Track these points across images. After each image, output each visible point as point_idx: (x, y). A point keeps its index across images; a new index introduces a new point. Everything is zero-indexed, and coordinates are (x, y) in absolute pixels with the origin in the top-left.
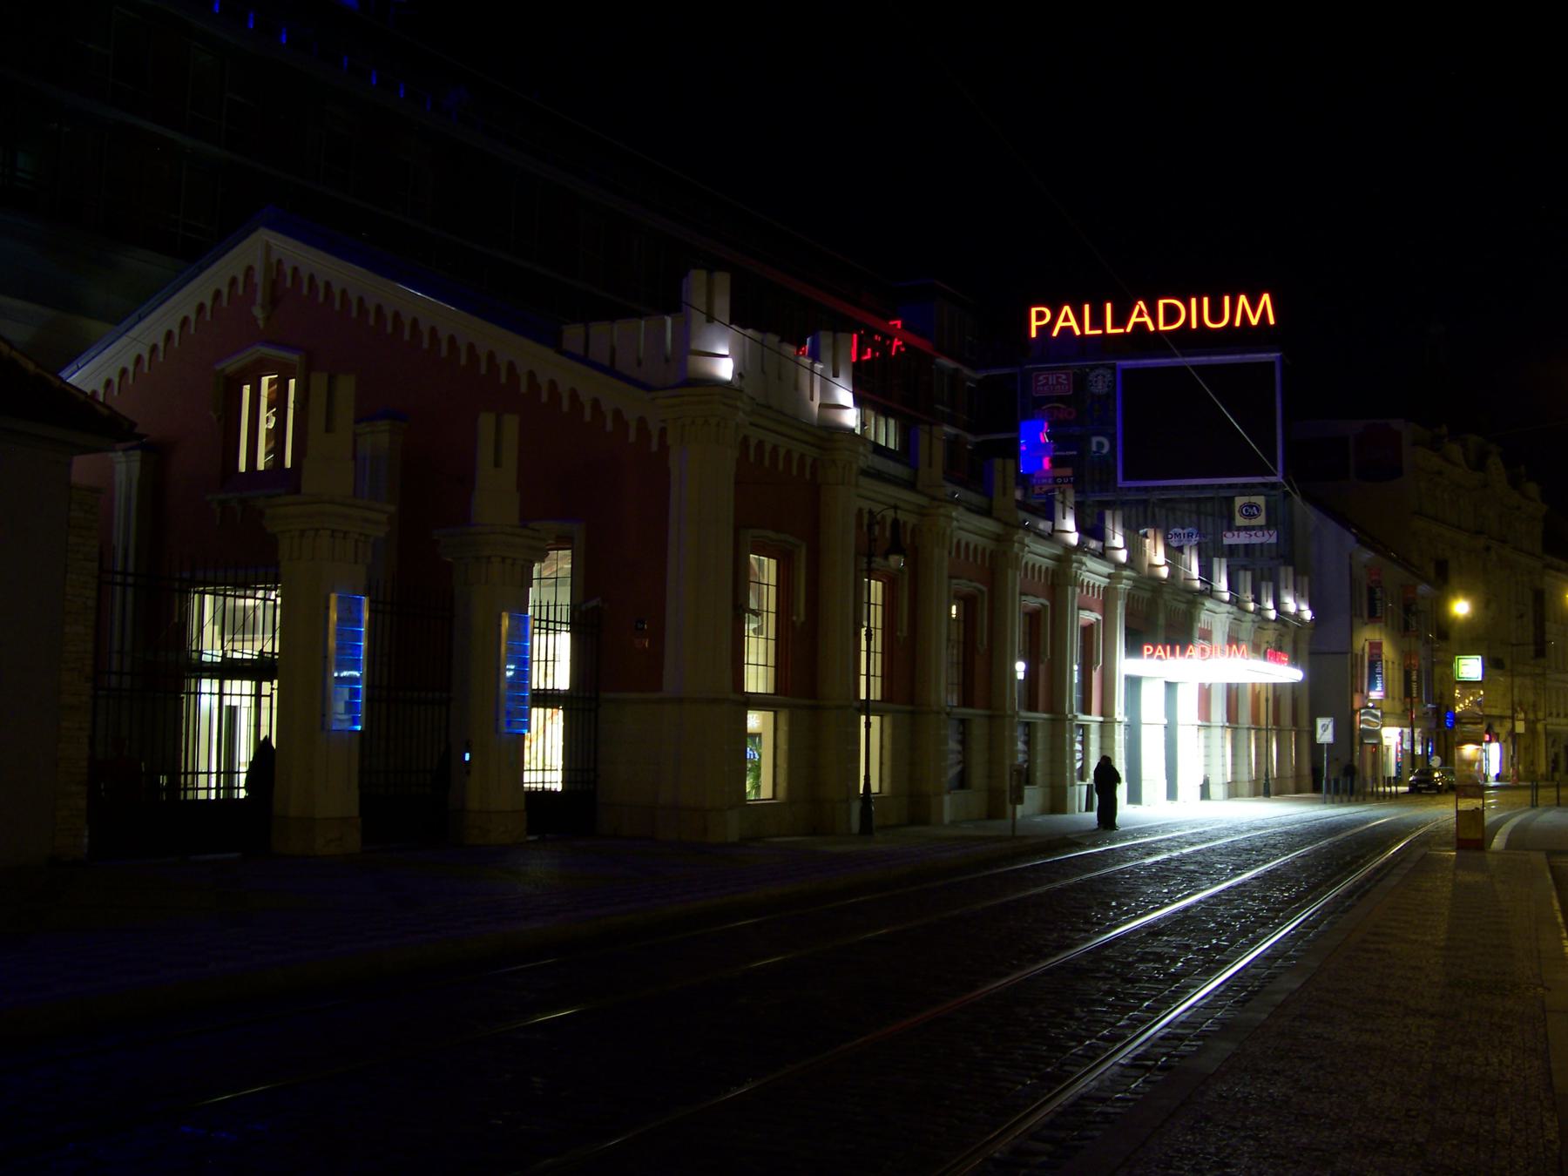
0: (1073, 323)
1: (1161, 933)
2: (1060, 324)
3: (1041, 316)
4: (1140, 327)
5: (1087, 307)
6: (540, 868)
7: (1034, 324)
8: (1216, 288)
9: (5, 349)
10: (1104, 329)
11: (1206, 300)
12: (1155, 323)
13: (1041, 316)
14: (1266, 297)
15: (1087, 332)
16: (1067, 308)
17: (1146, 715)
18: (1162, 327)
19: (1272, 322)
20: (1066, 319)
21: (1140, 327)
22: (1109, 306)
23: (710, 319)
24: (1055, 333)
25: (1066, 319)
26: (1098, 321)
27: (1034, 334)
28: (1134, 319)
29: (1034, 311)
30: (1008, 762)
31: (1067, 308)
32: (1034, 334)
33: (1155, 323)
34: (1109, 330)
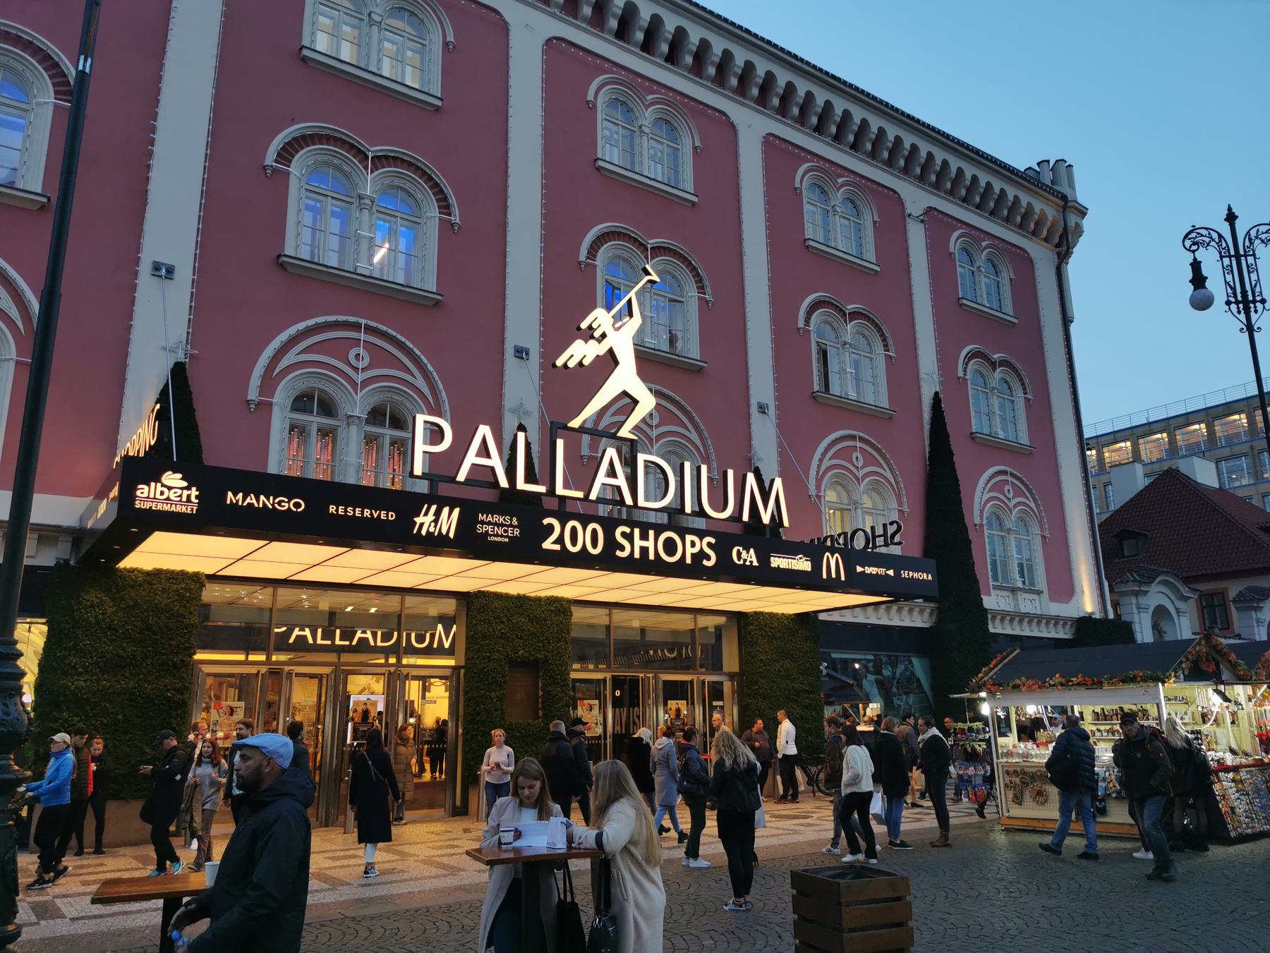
2: (471, 458)
10: (333, 641)
13: (435, 434)
16: (484, 431)
22: (392, 516)
24: (291, 641)
28: (601, 478)
31: (484, 431)
34: (560, 490)
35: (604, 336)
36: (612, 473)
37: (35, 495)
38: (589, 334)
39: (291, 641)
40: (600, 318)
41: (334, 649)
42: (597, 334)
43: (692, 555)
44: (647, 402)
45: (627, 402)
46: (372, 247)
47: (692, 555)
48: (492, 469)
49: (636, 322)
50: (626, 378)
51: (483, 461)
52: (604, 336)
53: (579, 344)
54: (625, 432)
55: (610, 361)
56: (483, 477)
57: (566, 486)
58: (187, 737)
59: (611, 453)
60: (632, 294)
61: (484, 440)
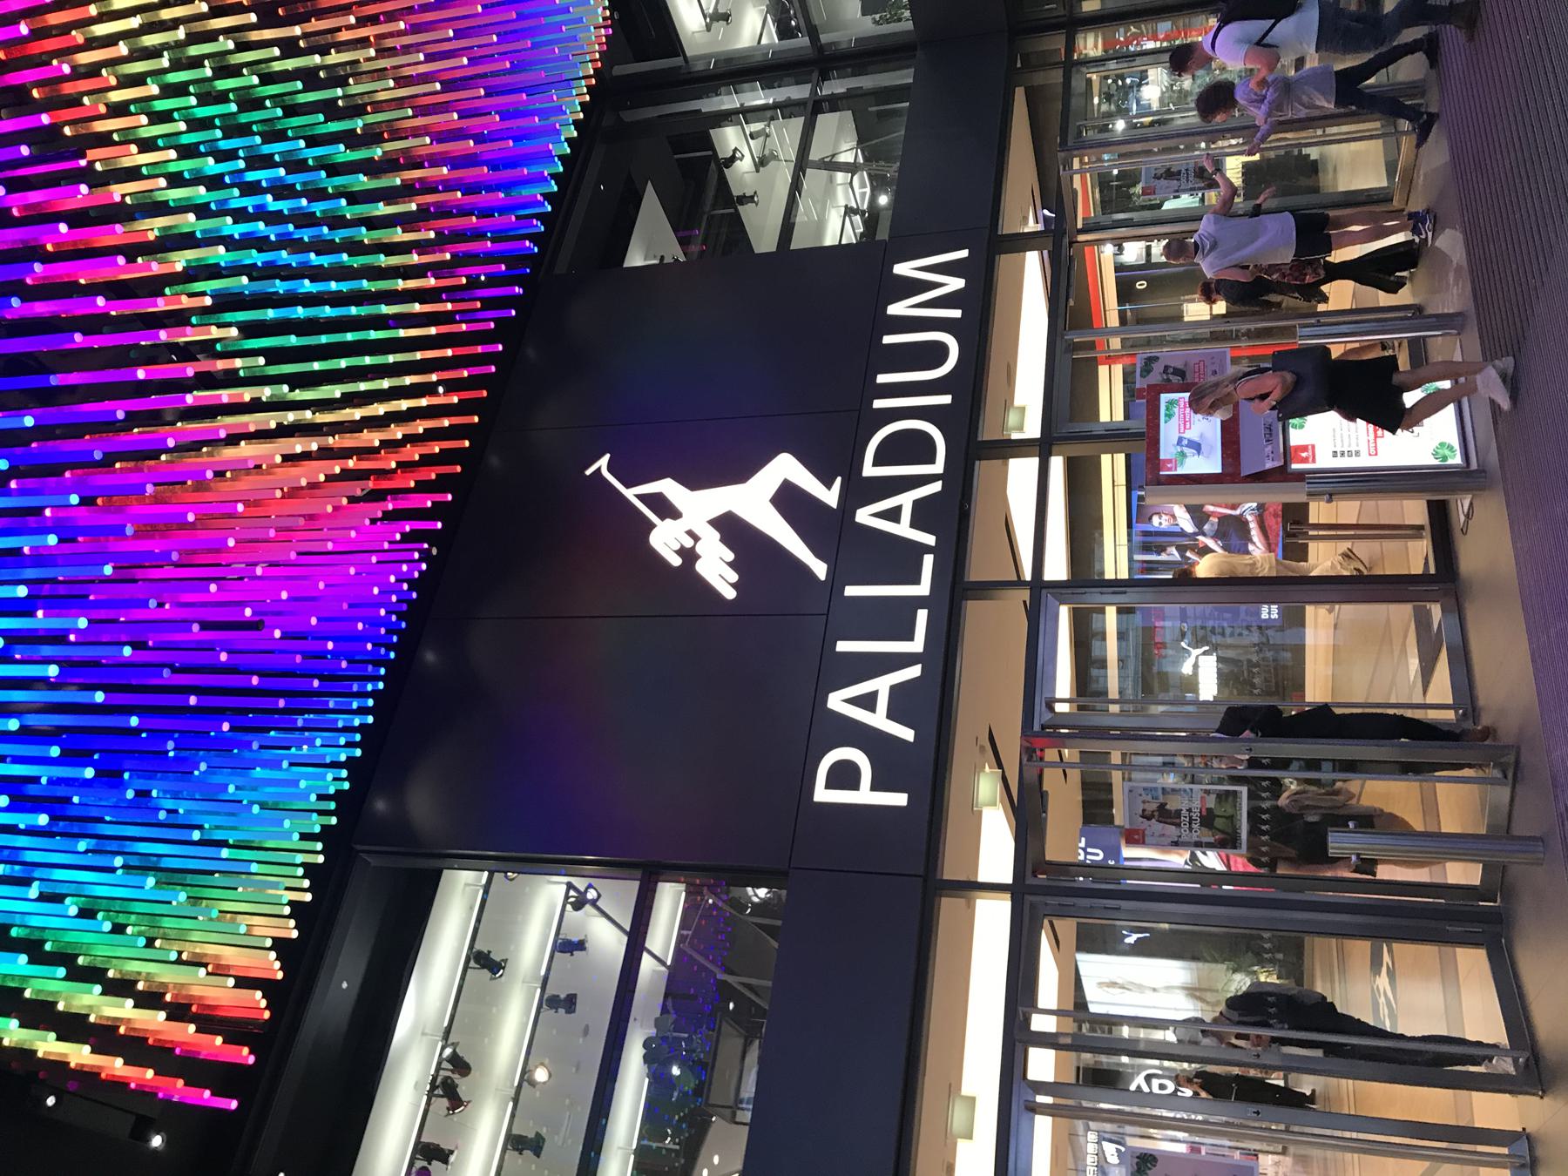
0: (882, 685)
2: (878, 720)
3: (844, 776)
4: (923, 515)
5: (843, 646)
6: (547, 1061)
7: (865, 795)
10: (918, 602)
11: (882, 379)
13: (844, 776)
14: (903, 269)
15: (917, 645)
16: (837, 701)
17: (1480, 1099)
18: (938, 467)
19: (964, 253)
20: (868, 702)
21: (923, 515)
22: (843, 646)
23: (1316, 190)
24: (907, 734)
25: (868, 702)
26: (895, 618)
27: (899, 799)
29: (823, 794)
31: (837, 701)
32: (899, 799)
34: (923, 589)
35: (690, 533)
37: (1477, 1125)
38: (689, 556)
39: (907, 734)
40: (665, 539)
41: (956, 591)
42: (689, 543)
44: (785, 468)
45: (789, 500)
46: (762, 908)
48: (893, 688)
49: (668, 487)
50: (752, 499)
51: (883, 703)
52: (690, 533)
53: (701, 567)
55: (731, 528)
58: (149, 1141)
59: (864, 516)
60: (630, 494)
61: (852, 701)
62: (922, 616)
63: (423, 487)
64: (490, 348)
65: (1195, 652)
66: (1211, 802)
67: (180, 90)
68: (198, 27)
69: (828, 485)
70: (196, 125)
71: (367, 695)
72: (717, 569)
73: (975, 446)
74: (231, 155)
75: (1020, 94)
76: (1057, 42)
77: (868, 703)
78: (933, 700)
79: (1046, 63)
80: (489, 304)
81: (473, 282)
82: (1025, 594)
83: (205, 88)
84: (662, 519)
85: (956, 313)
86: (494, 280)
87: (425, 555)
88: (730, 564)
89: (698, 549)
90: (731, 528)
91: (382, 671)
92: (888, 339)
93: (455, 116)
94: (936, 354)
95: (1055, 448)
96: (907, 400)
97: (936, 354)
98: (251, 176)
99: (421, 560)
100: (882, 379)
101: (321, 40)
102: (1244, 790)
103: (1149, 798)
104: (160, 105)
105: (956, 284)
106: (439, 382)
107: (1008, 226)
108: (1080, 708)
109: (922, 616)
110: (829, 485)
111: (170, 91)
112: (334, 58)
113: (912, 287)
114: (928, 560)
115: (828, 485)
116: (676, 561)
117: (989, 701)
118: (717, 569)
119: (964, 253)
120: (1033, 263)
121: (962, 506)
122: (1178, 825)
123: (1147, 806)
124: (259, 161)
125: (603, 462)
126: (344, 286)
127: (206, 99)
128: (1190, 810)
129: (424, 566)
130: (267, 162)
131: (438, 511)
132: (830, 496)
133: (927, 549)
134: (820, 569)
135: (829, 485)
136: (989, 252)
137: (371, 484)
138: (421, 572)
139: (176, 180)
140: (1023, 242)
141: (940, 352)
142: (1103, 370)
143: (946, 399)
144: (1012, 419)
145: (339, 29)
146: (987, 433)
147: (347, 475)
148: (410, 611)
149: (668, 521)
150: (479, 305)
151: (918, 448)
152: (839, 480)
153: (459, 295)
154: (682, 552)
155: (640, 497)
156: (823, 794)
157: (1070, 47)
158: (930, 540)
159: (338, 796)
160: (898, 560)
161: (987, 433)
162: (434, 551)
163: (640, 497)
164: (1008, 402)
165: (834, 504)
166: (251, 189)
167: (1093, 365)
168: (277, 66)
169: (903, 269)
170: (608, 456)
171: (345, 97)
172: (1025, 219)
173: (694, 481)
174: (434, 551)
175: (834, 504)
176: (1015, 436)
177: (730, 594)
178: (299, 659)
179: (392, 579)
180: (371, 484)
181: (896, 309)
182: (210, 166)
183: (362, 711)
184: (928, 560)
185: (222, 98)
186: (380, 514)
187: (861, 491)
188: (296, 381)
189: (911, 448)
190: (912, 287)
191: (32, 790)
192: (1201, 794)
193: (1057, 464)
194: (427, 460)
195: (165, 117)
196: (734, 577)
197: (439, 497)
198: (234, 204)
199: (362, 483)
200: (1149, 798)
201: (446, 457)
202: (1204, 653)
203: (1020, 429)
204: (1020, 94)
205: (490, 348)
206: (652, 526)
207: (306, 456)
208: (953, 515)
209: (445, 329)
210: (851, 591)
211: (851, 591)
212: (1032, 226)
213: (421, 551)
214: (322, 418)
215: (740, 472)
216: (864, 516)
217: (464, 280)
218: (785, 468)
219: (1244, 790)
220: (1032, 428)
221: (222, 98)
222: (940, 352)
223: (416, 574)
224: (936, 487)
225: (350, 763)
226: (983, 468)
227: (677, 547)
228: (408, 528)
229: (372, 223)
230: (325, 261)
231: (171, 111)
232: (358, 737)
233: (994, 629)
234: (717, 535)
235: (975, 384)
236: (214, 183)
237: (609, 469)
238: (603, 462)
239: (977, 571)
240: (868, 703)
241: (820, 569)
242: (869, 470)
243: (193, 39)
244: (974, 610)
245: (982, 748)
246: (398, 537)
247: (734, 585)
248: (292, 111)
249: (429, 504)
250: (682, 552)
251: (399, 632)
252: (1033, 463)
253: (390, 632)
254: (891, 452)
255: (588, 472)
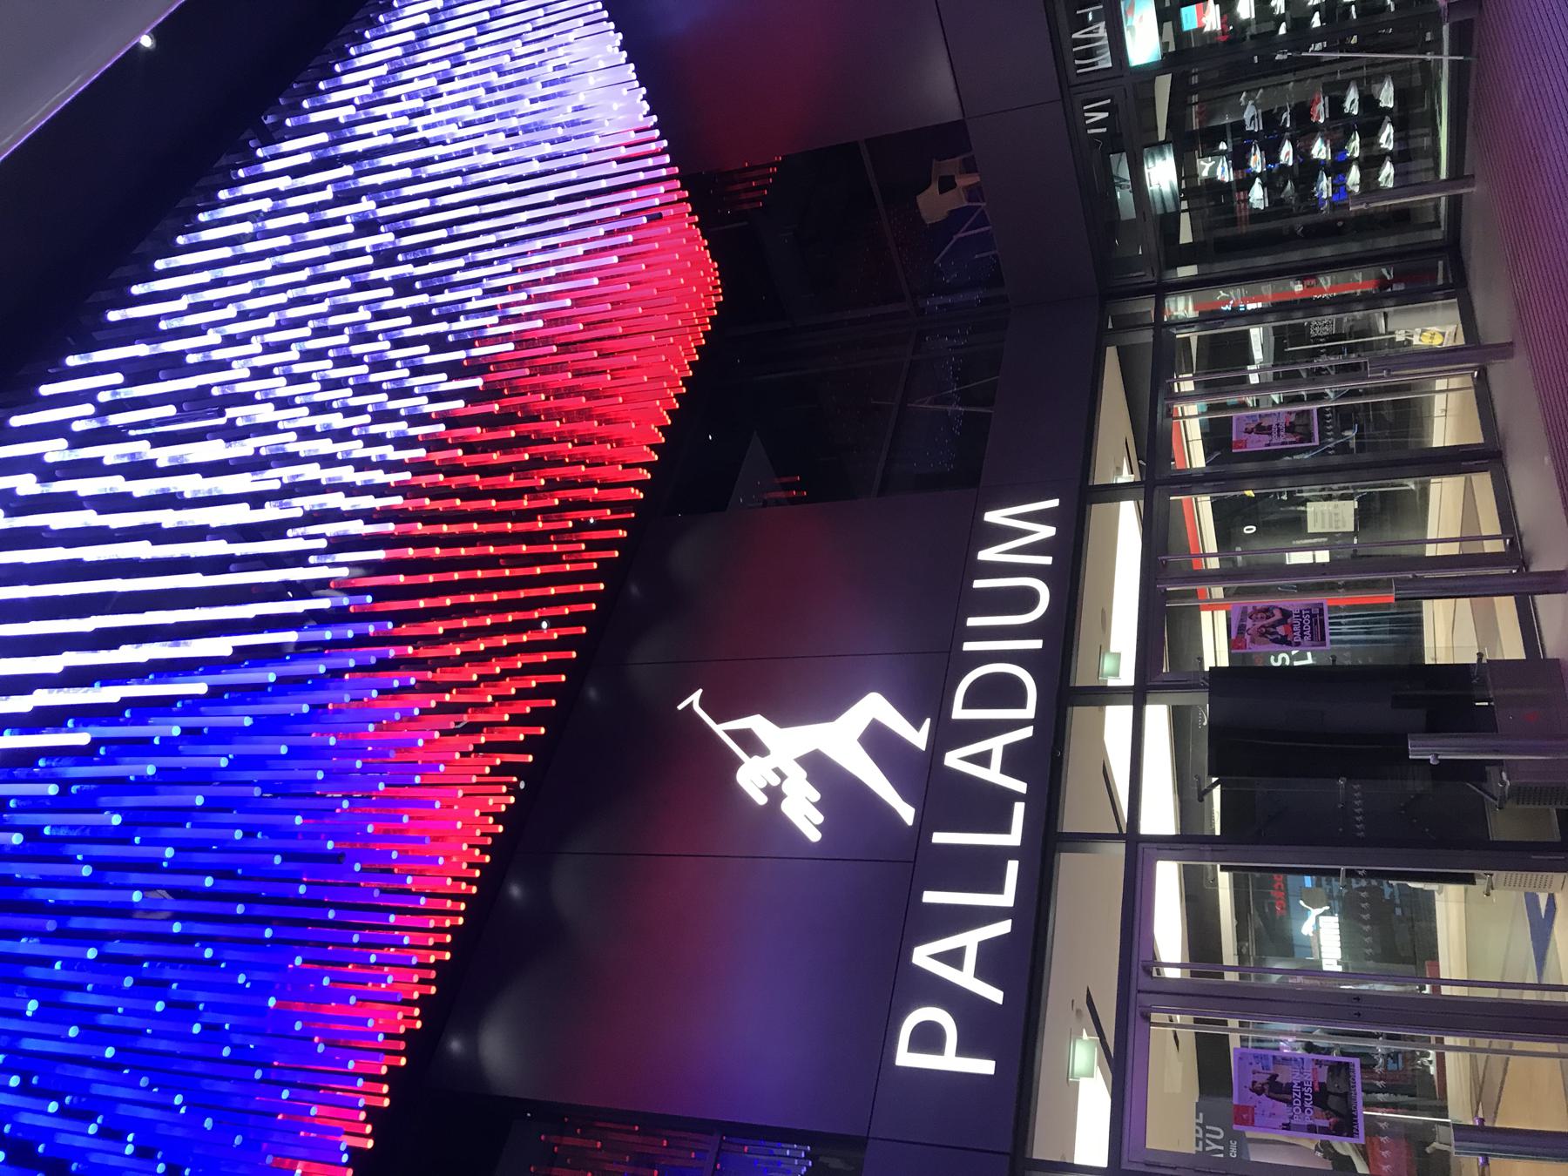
0: (970, 940)
1: (1378, 65)
2: (965, 978)
4: (1014, 761)
5: (930, 897)
7: (949, 1061)
8: (907, 798)
9: (415, 15)
10: (1006, 853)
11: (972, 622)
12: (994, 915)
13: (928, 1038)
14: (993, 517)
15: (1007, 899)
16: (923, 956)
18: (1029, 712)
19: (1055, 503)
21: (1014, 761)
22: (930, 897)
24: (996, 995)
25: (983, 759)
26: (981, 870)
27: (986, 1067)
28: (993, 774)
29: (905, 1058)
30: (1481, 872)
31: (923, 956)
32: (986, 1067)
33: (994, 915)
34: (1014, 838)
35: (777, 771)
36: (983, 759)
38: (776, 795)
39: (996, 995)
40: (752, 777)
41: (1047, 844)
43: (963, 1050)
44: (875, 708)
45: (877, 741)
47: (963, 1050)
49: (757, 723)
50: (841, 738)
52: (777, 771)
53: (787, 807)
54: (919, 738)
55: (818, 767)
56: (991, 962)
57: (999, 889)
59: (954, 759)
60: (719, 729)
61: (938, 957)
62: (1013, 867)
63: (517, 720)
64: (592, 587)
65: (1314, 912)
66: (1323, 1076)
67: (320, 354)
68: (341, 299)
69: (917, 726)
70: (329, 385)
71: (445, 931)
72: (803, 811)
73: (1067, 694)
74: (360, 410)
75: (1111, 354)
76: (1147, 306)
77: (954, 959)
78: (1022, 960)
79: (1134, 323)
80: (593, 545)
81: (581, 526)
82: (1120, 848)
83: (343, 352)
84: (750, 754)
85: (1047, 560)
86: (602, 525)
87: (513, 788)
88: (816, 805)
89: (785, 789)
90: (818, 767)
91: (463, 906)
92: (978, 584)
93: (570, 375)
94: (1027, 599)
95: (1149, 697)
96: (998, 644)
97: (1027, 599)
98: (375, 429)
99: (508, 794)
100: (972, 622)
101: (453, 309)
102: (1356, 1062)
103: (1259, 1067)
104: (298, 369)
105: (1046, 532)
106: (541, 619)
107: (1100, 477)
108: (1193, 974)
109: (1013, 867)
110: (918, 727)
111: (308, 356)
112: (463, 324)
113: (1001, 534)
114: (1019, 809)
115: (917, 726)
116: (762, 800)
117: (1083, 961)
118: (803, 811)
119: (1055, 503)
120: (1128, 514)
121: (1054, 753)
122: (1289, 1103)
123: (1257, 1077)
124: (382, 416)
125: (695, 698)
126: (456, 529)
127: (341, 362)
128: (1301, 1084)
129: (512, 800)
130: (393, 416)
131: (529, 745)
132: (919, 738)
133: (1017, 796)
134: (907, 813)
135: (918, 727)
136: (1080, 503)
137: (465, 718)
138: (508, 805)
139: (306, 434)
140: (1115, 493)
141: (1030, 598)
142: (1206, 616)
143: (1037, 644)
144: (1108, 664)
145: (469, 300)
146: (1081, 679)
147: (443, 708)
148: (498, 847)
149: (756, 758)
150: (583, 546)
151: (1008, 692)
152: (928, 721)
153: (566, 537)
154: (768, 790)
155: (729, 733)
156: (905, 1058)
157: (1160, 309)
158: (1020, 787)
159: (410, 1034)
160: (988, 808)
161: (1081, 679)
162: (522, 785)
163: (729, 733)
164: (1103, 648)
165: (923, 746)
166: (379, 440)
167: (1198, 609)
168: (408, 333)
169: (993, 517)
170: (700, 691)
171: (468, 358)
172: (1119, 471)
173: (783, 718)
174: (522, 785)
175: (923, 746)
176: (1112, 682)
177: (815, 836)
178: (278, 860)
179: (477, 813)
180: (465, 718)
181: (986, 555)
182: (337, 421)
183: (440, 947)
184: (1019, 809)
185: (357, 360)
186: (471, 748)
187: (949, 734)
188: (399, 618)
189: (1002, 691)
190: (1001, 534)
191: (105, 1019)
192: (1312, 1065)
193: (1157, 716)
194: (523, 694)
195: (305, 378)
196: (819, 818)
197: (532, 731)
198: (355, 455)
199: (456, 717)
200: (1259, 1067)
201: (543, 691)
202: (1324, 914)
203: (1116, 675)
204: (1111, 354)
205: (592, 587)
206: (739, 763)
207: (405, 689)
208: (1044, 760)
209: (549, 569)
210: (939, 838)
211: (939, 838)
212: (1126, 477)
213: (508, 784)
214: (425, 653)
215: (830, 708)
216: (954, 759)
217: (570, 524)
218: (875, 708)
219: (1356, 1062)
220: (1126, 677)
221: (357, 360)
222: (1030, 598)
223: (503, 808)
224: (1028, 732)
225: (424, 1001)
226: (1079, 715)
227: (764, 785)
228: (498, 762)
229: (486, 471)
230: (441, 505)
231: (310, 373)
232: (433, 974)
233: (1090, 882)
234: (804, 774)
235: (1065, 631)
236: (343, 435)
237: (702, 705)
238: (695, 698)
239: (1071, 822)
240: (954, 959)
241: (907, 813)
242: (959, 713)
243: (338, 310)
244: (1068, 863)
245: (1079, 1012)
246: (487, 770)
247: (819, 827)
248: (418, 370)
249: (522, 737)
250: (768, 790)
251: (481, 866)
252: (1127, 711)
253: (471, 866)
254: (982, 694)
255: (680, 707)
